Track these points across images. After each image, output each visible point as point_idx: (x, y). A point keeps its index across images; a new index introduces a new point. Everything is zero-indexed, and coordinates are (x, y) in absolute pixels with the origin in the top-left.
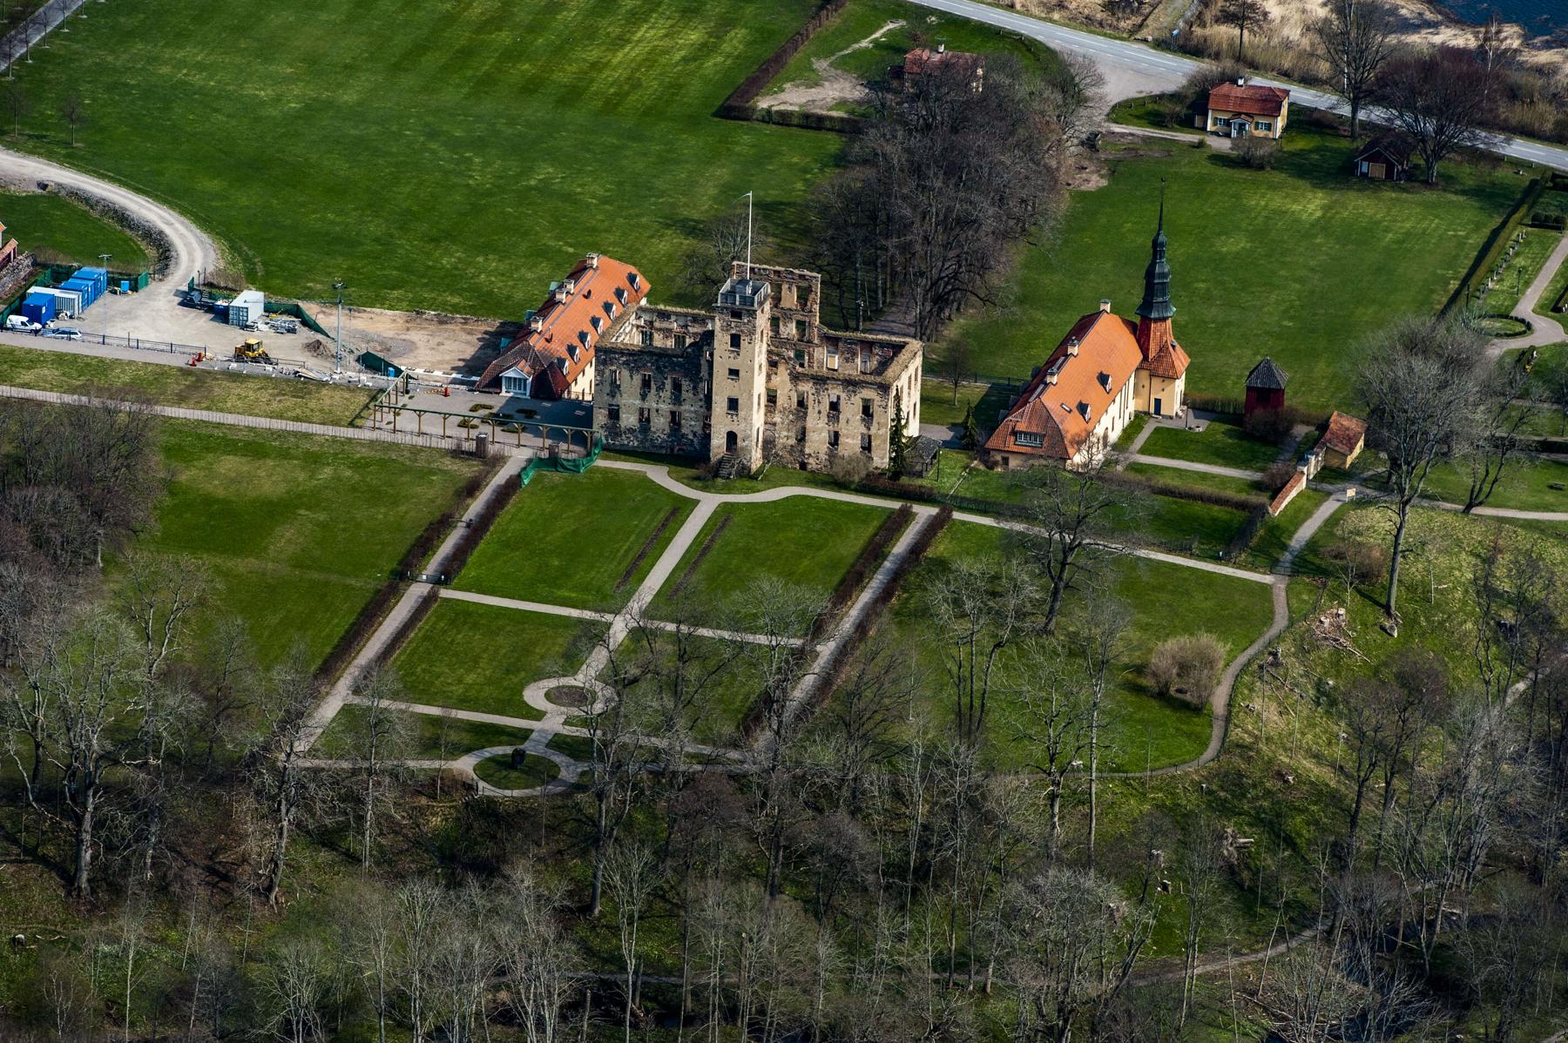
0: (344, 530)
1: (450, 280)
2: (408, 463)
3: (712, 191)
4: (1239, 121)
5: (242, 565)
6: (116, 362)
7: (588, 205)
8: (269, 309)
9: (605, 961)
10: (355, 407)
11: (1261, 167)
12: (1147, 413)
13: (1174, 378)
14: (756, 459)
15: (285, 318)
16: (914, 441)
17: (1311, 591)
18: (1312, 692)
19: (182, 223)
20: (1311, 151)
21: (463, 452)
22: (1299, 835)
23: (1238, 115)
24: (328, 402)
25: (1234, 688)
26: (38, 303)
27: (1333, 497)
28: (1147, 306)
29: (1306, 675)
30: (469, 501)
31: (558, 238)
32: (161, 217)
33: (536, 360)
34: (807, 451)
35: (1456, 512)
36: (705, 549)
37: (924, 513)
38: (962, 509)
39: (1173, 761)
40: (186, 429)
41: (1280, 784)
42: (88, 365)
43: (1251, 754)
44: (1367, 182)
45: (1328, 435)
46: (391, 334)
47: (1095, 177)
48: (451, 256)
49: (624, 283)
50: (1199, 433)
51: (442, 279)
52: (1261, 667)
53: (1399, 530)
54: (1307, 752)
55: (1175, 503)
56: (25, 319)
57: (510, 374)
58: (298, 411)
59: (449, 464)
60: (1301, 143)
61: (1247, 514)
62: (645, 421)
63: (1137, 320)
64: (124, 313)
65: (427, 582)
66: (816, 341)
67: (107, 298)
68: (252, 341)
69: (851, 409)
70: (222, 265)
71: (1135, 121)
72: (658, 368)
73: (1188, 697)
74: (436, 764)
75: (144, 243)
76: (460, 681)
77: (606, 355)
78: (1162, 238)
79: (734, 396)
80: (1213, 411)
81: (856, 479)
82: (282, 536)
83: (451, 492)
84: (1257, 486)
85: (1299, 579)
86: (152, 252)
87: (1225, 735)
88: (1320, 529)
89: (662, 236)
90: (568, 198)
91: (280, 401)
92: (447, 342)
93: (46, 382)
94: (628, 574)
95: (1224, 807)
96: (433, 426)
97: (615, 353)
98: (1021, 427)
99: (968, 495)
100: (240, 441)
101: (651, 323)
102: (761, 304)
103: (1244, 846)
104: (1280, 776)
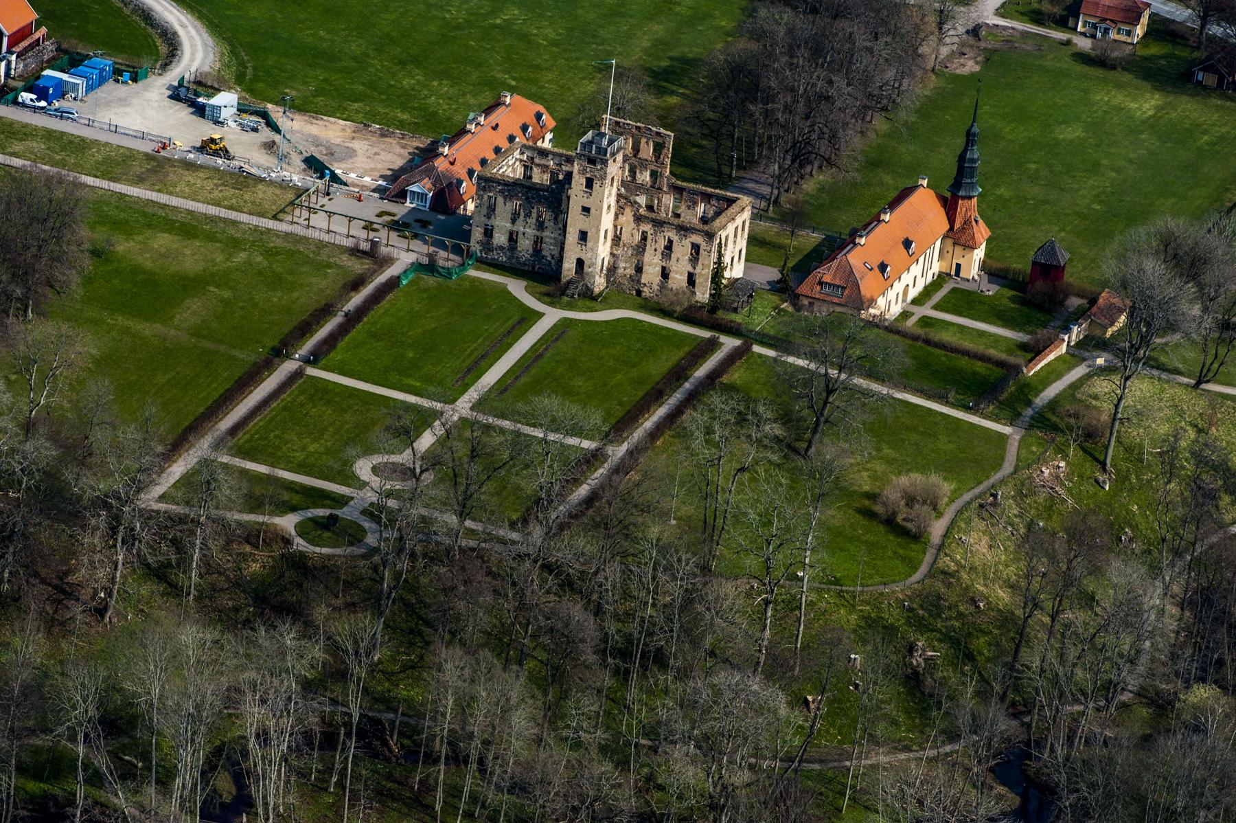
0: (242, 308)
1: (405, 99)
2: (311, 255)
3: (646, 44)
4: (1104, 26)
5: (148, 329)
6: (95, 142)
7: (539, 45)
8: (241, 110)
9: (376, 700)
10: (281, 203)
11: (1113, 68)
12: (949, 275)
13: (973, 248)
14: (599, 283)
15: (253, 118)
16: (734, 282)
17: (1040, 444)
18: (1022, 531)
19: (195, 27)
20: (1161, 57)
21: (359, 251)
22: (981, 653)
23: (1104, 20)
24: (261, 195)
25: (953, 523)
26: (46, 85)
27: (1086, 363)
28: (957, 185)
29: (1020, 516)
30: (352, 294)
31: (505, 71)
32: (179, 20)
33: (437, 180)
34: (643, 281)
35: (1187, 385)
36: (538, 356)
37: (729, 343)
38: (763, 343)
39: (885, 580)
40: (136, 207)
41: (972, 608)
42: (71, 142)
43: (952, 580)
44: (1201, 89)
45: (1094, 309)
46: (338, 141)
47: (971, 63)
48: (413, 78)
49: (530, 119)
50: (989, 296)
51: (399, 97)
52: (981, 506)
53: (1120, 400)
54: (1005, 582)
55: (946, 356)
56: (34, 97)
57: (414, 188)
58: (234, 201)
59: (347, 261)
60: (1154, 50)
61: (1005, 371)
62: (513, 238)
63: (948, 195)
64: (120, 100)
65: (298, 360)
66: (665, 189)
67: (110, 86)
68: (216, 136)
69: (682, 250)
70: (218, 65)
71: (1020, 17)
72: (527, 198)
73: (909, 525)
74: (260, 519)
75: (160, 40)
76: (304, 448)
77: (486, 183)
78: (976, 129)
79: (584, 229)
80: (1005, 278)
81: (678, 309)
82: (189, 308)
83: (340, 284)
84: (1024, 347)
85: (1032, 432)
86: (163, 49)
87: (935, 561)
88: (1065, 390)
89: (593, 79)
90: (525, 37)
91: (221, 191)
92: (382, 153)
93: (32, 153)
94: (469, 370)
95: (920, 623)
96: (339, 226)
97: (493, 182)
98: (827, 279)
99: (772, 332)
100: (178, 221)
101: (532, 159)
102: (613, 154)
103: (931, 658)
104: (973, 601)
